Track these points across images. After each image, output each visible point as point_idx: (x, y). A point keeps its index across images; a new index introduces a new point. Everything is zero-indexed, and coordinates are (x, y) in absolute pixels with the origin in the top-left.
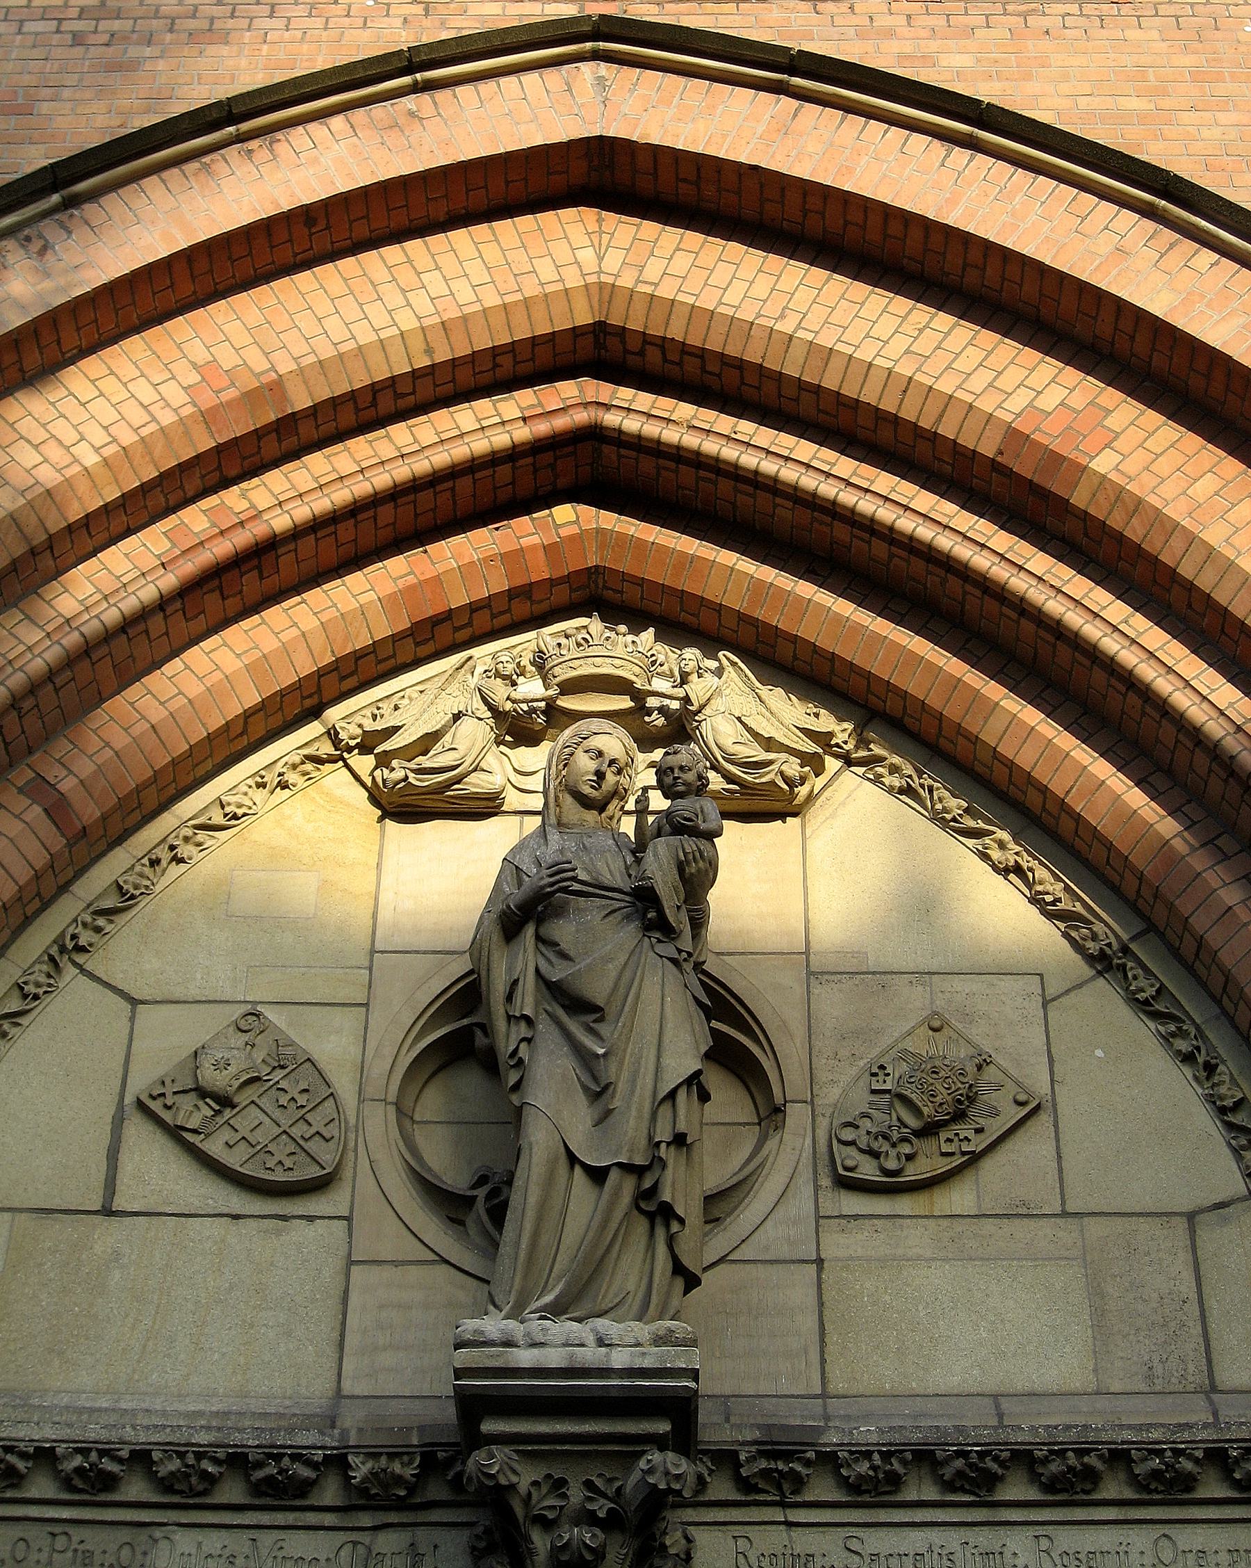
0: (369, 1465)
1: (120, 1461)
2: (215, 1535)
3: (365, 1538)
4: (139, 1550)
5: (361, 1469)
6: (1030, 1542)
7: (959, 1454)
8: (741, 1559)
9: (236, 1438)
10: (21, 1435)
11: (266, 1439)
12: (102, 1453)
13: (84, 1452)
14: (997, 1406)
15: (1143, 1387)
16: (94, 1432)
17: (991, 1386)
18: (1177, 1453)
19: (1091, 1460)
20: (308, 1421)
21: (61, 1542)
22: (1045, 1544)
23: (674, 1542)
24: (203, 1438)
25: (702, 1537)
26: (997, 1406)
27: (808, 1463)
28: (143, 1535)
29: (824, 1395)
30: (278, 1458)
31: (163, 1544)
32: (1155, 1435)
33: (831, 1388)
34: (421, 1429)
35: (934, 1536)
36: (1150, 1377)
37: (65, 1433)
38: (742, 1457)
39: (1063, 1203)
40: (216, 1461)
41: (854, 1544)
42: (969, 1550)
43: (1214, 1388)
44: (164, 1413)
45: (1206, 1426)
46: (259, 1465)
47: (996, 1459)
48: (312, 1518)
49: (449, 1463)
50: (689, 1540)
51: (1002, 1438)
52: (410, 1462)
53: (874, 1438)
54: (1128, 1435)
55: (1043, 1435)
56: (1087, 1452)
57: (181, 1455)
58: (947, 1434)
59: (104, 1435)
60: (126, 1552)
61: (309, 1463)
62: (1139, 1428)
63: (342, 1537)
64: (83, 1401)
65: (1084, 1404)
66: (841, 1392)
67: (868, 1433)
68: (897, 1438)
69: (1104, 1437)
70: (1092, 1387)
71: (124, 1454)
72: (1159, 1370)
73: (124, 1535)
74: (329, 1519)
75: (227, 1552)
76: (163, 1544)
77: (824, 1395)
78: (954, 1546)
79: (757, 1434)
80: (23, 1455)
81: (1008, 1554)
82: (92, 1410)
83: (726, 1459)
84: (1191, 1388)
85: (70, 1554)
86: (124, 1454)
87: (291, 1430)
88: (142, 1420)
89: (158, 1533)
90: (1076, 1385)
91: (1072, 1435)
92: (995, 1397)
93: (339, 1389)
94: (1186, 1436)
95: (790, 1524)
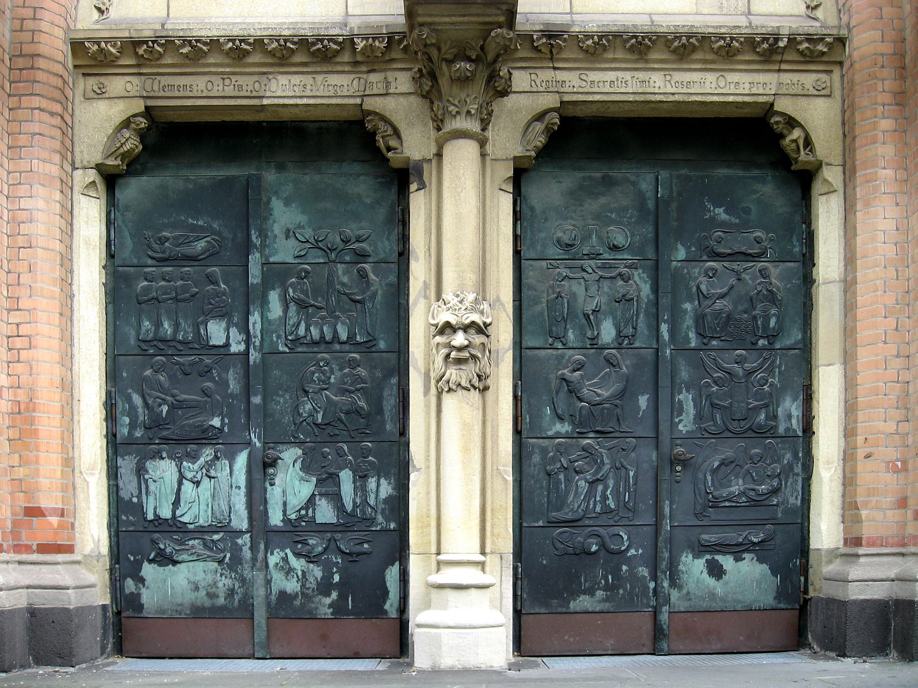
0: (364, 42)
1: (250, 44)
2: (296, 76)
3: (365, 76)
4: (262, 84)
5: (360, 45)
6: (662, 77)
7: (633, 37)
8: (533, 83)
9: (303, 32)
10: (203, 34)
11: (316, 32)
12: (241, 41)
13: (233, 41)
14: (651, 18)
15: (718, 12)
16: (236, 32)
17: (648, 10)
18: (732, 39)
19: (693, 40)
20: (334, 25)
21: (227, 82)
22: (668, 78)
23: (503, 72)
24: (286, 33)
25: (516, 74)
26: (651, 18)
27: (565, 40)
28: (264, 78)
29: (571, 13)
30: (322, 41)
31: (273, 81)
32: (723, 31)
33: (574, 10)
34: (387, 26)
35: (620, 74)
36: (721, 7)
37: (222, 33)
38: (535, 37)
39: (571, 8)
40: (294, 43)
41: (584, 77)
42: (634, 80)
43: (749, 13)
44: (267, 23)
45: (746, 27)
46: (314, 44)
47: (650, 40)
48: (339, 68)
49: (400, 41)
50: (511, 74)
51: (654, 30)
52: (383, 40)
53: (595, 29)
54: (711, 30)
55: (672, 30)
56: (692, 37)
57: (278, 41)
58: (628, 28)
59: (241, 33)
60: (257, 85)
61: (336, 43)
62: (717, 27)
63: (353, 76)
64: (229, 20)
65: (691, 18)
66: (579, 11)
67: (592, 27)
68: (606, 29)
69: (700, 31)
70: (694, 11)
71: (251, 41)
72: (725, 4)
73: (256, 78)
74: (347, 68)
75: (303, 83)
76: (273, 81)
77: (571, 13)
78: (629, 78)
79: (542, 28)
80: (205, 44)
81: (652, 82)
82: (234, 24)
83: (528, 38)
84: (739, 13)
85: (232, 86)
86: (251, 41)
87: (327, 28)
88: (256, 26)
89: (270, 77)
90: (687, 10)
91: (686, 30)
92: (650, 14)
93: (347, 12)
94: (737, 31)
95: (555, 68)
